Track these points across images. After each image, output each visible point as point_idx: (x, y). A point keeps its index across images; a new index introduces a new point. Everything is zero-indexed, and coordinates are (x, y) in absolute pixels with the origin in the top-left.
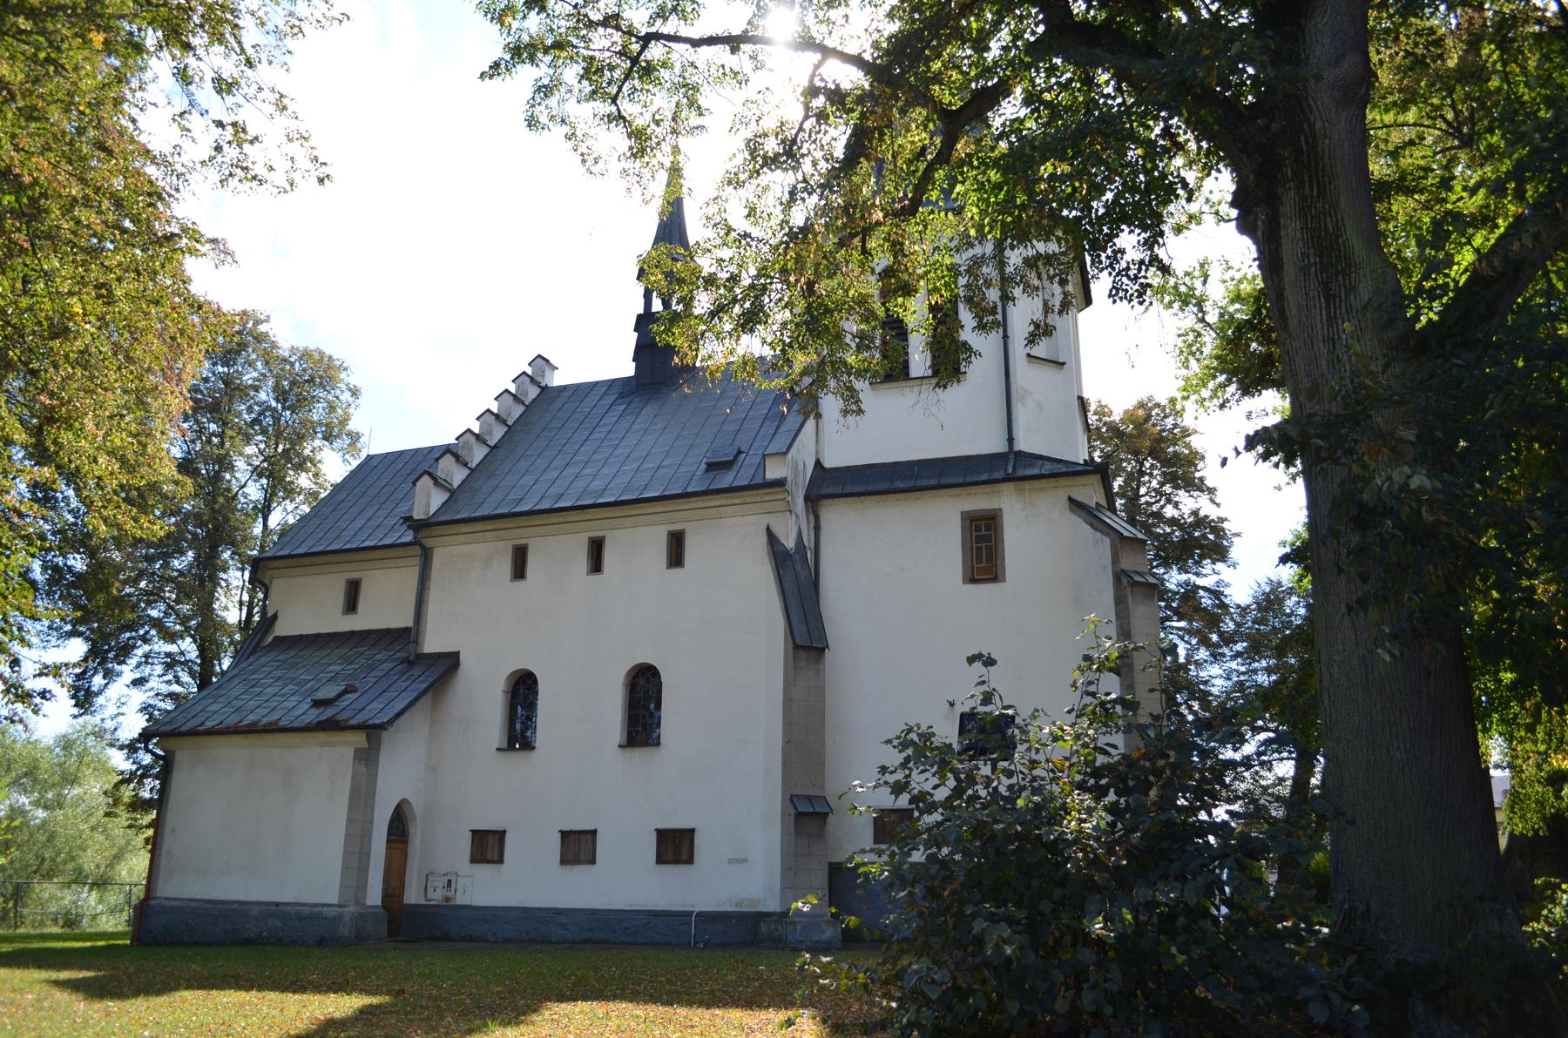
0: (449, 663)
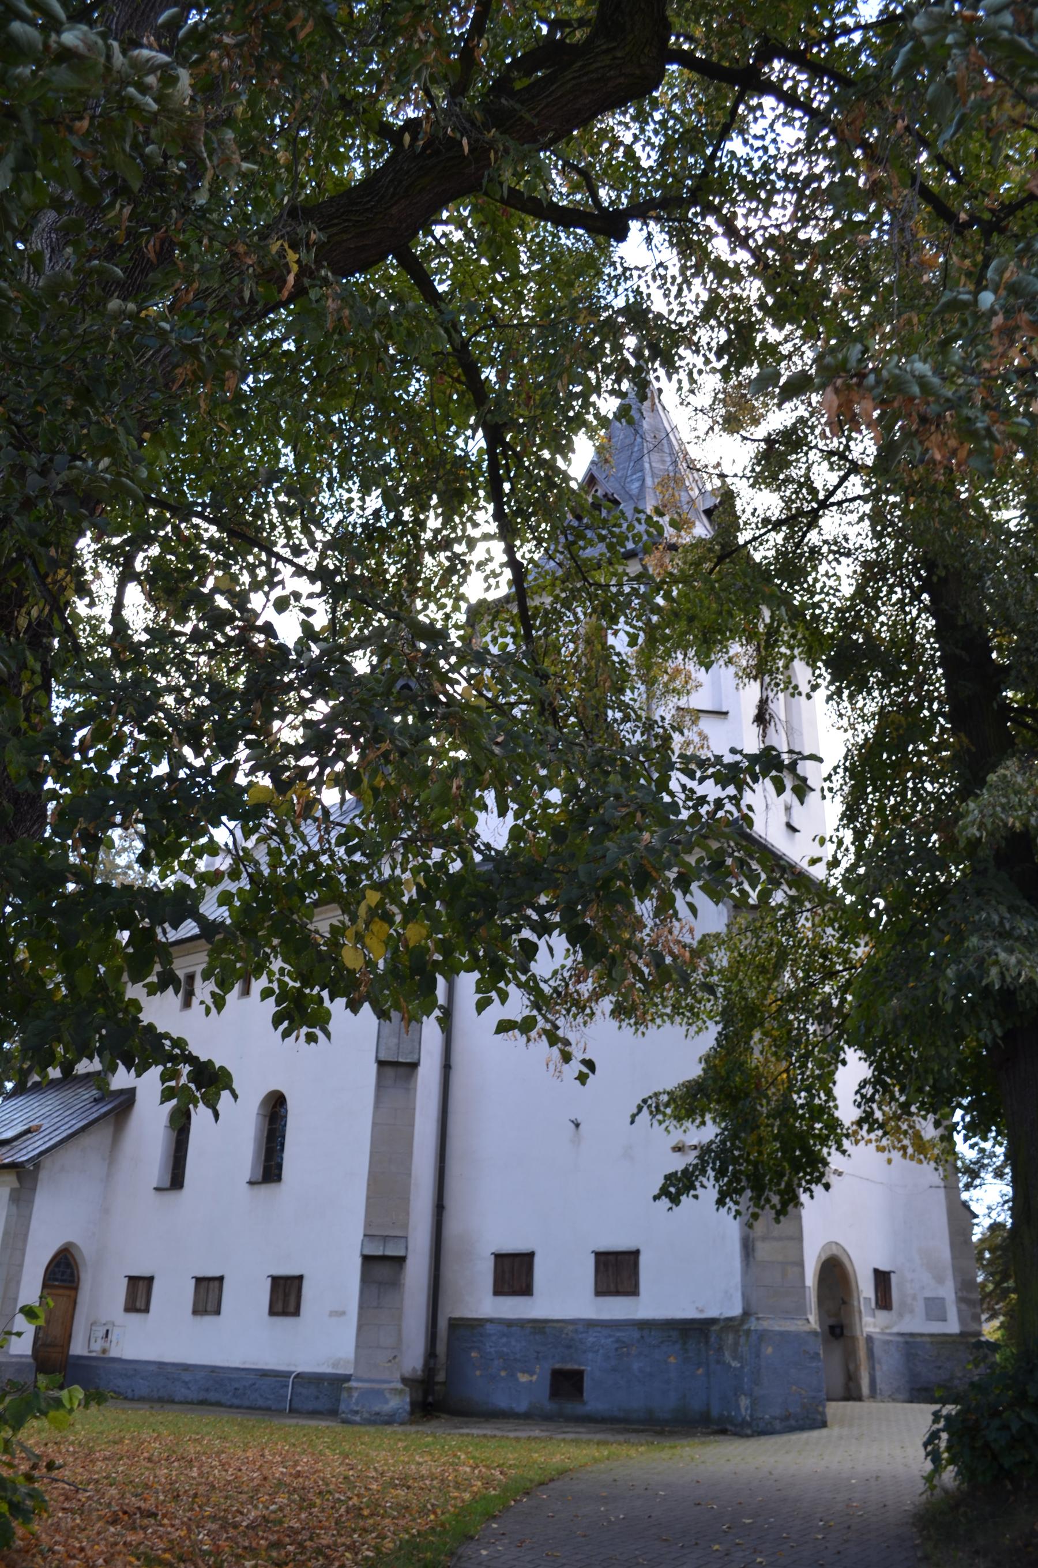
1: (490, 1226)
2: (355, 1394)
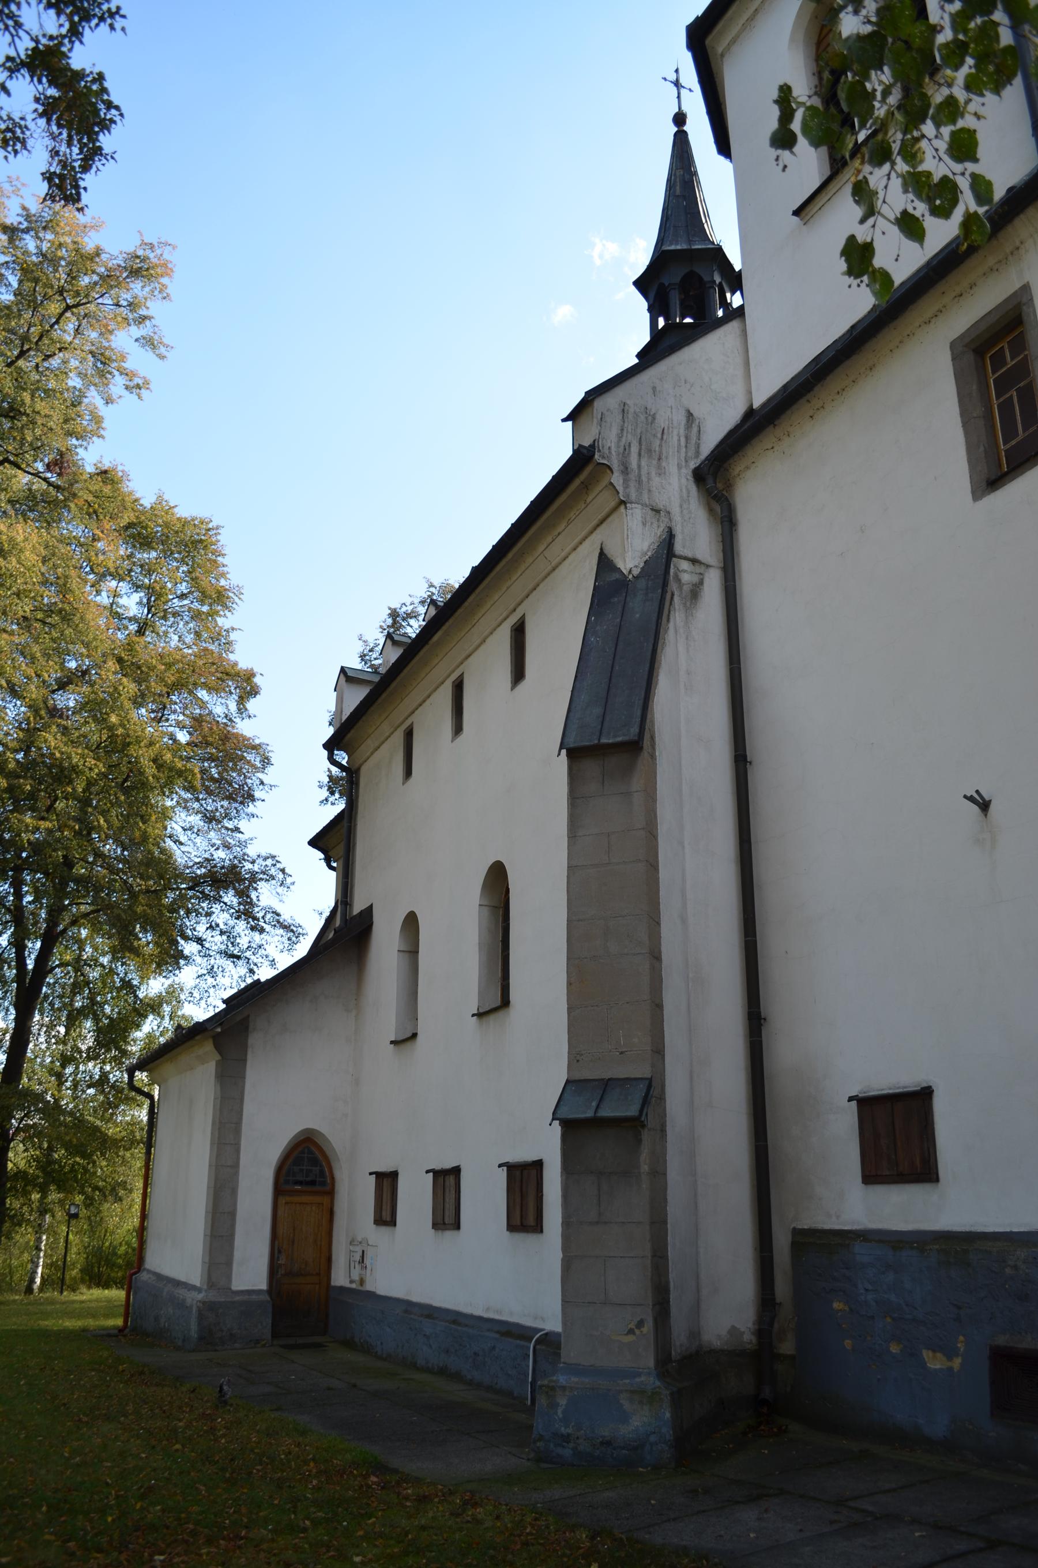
1: (851, 1043)
2: (563, 1402)
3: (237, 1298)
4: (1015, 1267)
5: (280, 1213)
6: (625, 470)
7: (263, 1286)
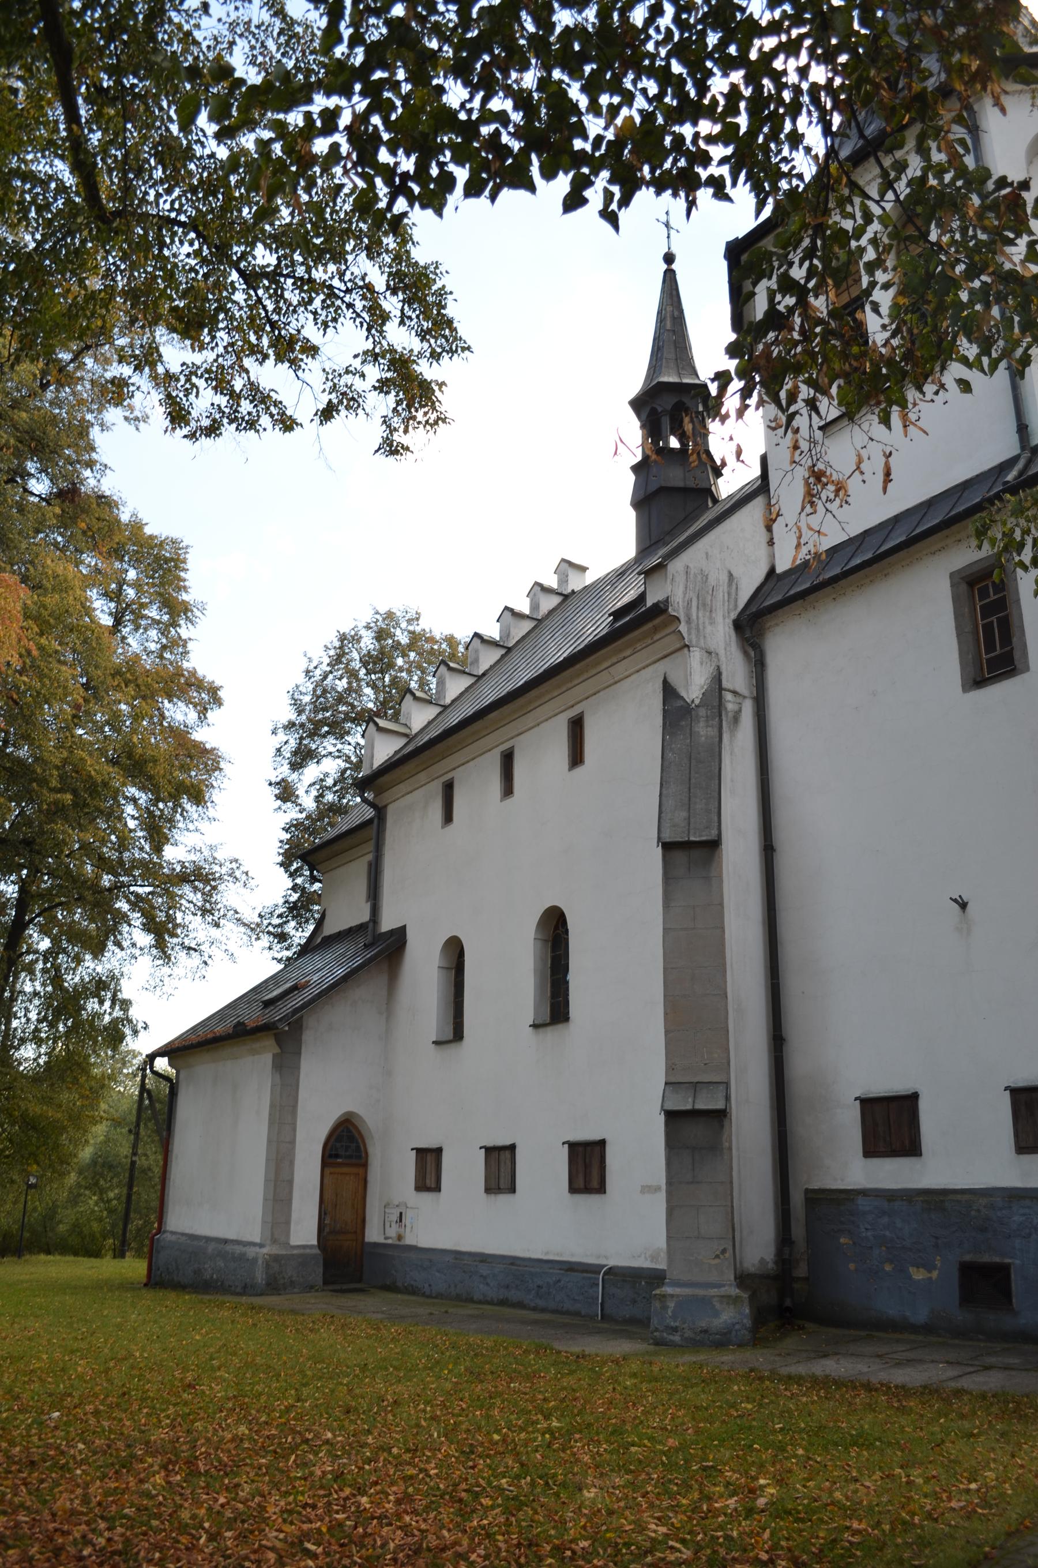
0: (399, 936)
1: (853, 1057)
2: (671, 1305)
3: (295, 1252)
4: (979, 1211)
5: (326, 1181)
6: (689, 621)
7: (315, 1242)
